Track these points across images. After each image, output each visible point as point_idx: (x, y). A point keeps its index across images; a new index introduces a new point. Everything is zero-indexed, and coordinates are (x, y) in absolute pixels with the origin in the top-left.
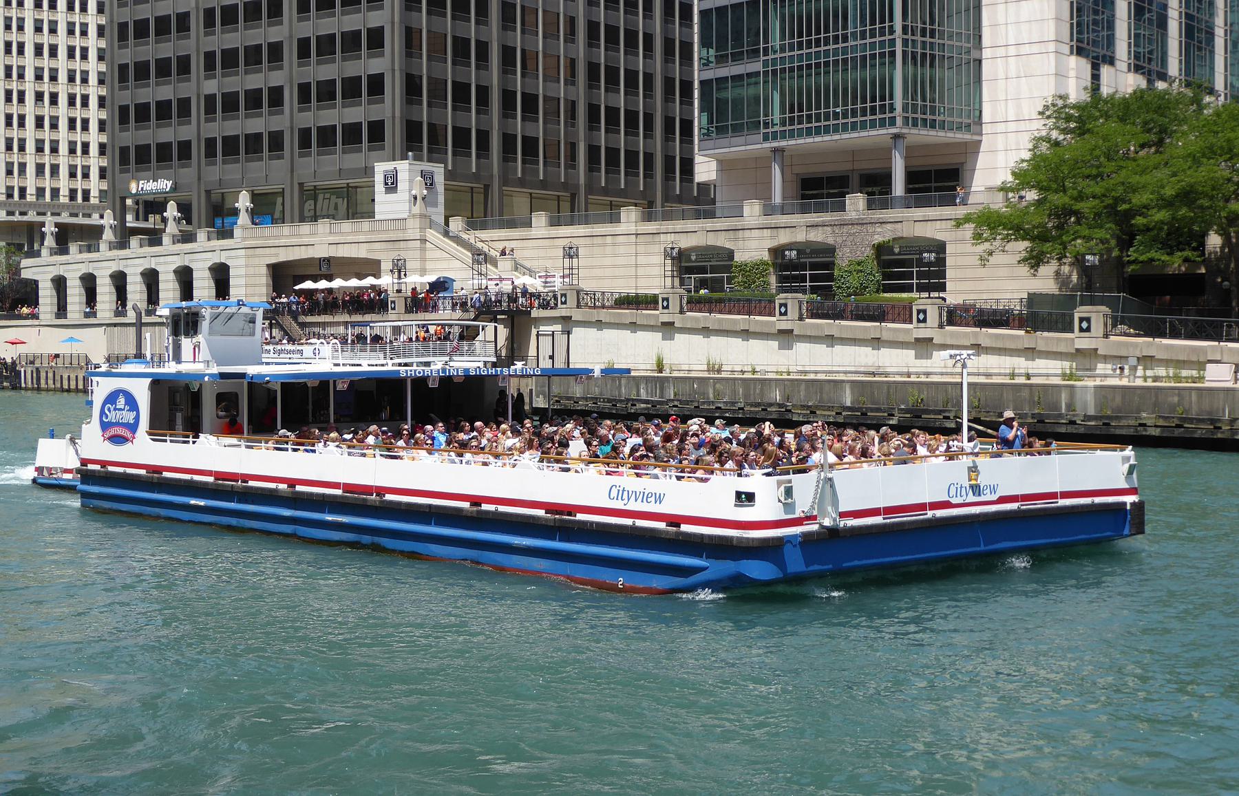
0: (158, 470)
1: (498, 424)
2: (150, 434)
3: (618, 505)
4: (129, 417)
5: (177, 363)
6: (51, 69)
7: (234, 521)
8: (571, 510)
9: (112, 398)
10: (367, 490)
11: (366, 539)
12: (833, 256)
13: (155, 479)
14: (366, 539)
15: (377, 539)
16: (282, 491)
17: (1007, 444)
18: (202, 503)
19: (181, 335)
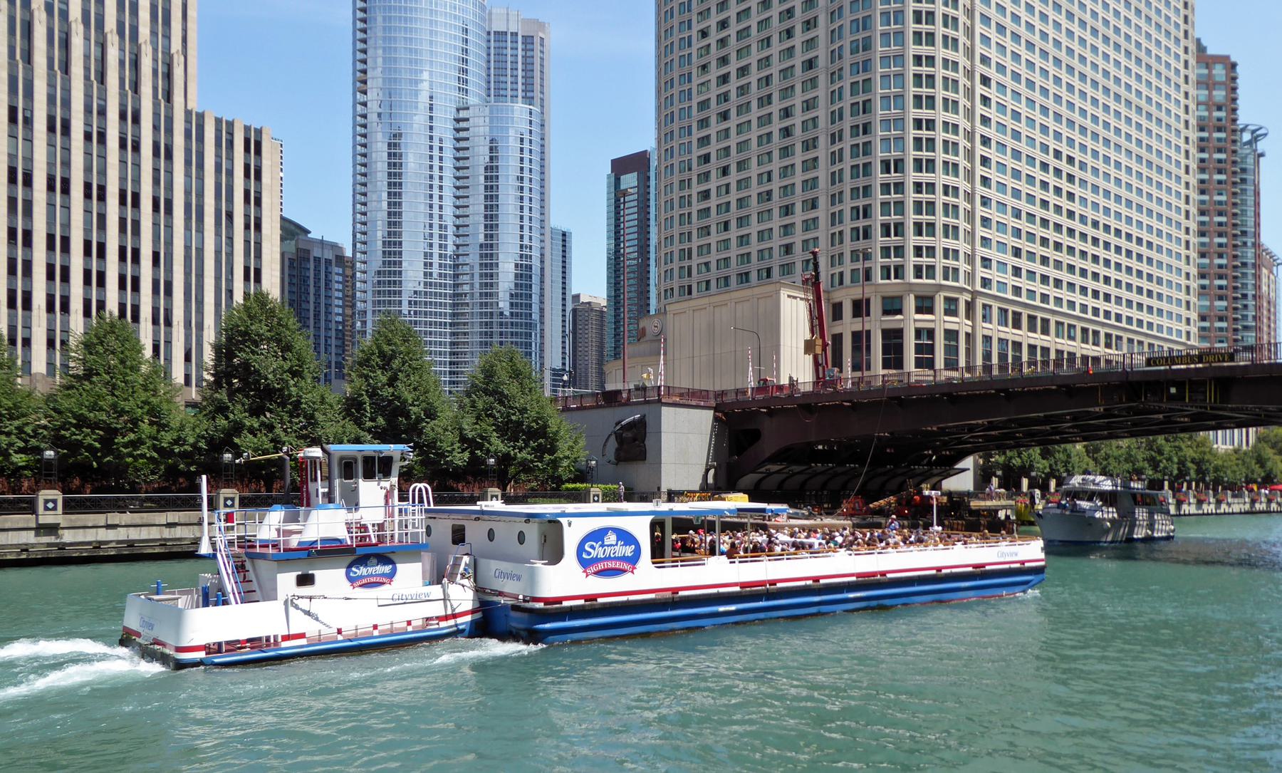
0: (675, 591)
1: (999, 532)
2: (653, 563)
3: (1002, 560)
4: (628, 551)
5: (349, 510)
6: (947, 332)
7: (762, 615)
8: (983, 566)
9: (625, 537)
10: (874, 574)
11: (874, 603)
12: (373, 458)
13: (672, 600)
14: (874, 603)
15: (881, 602)
16: (810, 586)
17: (911, 543)
18: (733, 608)
19: (357, 477)
